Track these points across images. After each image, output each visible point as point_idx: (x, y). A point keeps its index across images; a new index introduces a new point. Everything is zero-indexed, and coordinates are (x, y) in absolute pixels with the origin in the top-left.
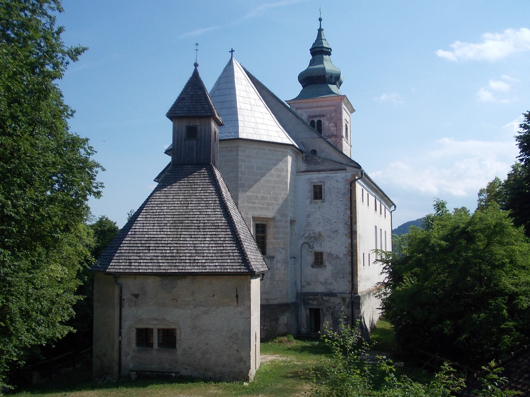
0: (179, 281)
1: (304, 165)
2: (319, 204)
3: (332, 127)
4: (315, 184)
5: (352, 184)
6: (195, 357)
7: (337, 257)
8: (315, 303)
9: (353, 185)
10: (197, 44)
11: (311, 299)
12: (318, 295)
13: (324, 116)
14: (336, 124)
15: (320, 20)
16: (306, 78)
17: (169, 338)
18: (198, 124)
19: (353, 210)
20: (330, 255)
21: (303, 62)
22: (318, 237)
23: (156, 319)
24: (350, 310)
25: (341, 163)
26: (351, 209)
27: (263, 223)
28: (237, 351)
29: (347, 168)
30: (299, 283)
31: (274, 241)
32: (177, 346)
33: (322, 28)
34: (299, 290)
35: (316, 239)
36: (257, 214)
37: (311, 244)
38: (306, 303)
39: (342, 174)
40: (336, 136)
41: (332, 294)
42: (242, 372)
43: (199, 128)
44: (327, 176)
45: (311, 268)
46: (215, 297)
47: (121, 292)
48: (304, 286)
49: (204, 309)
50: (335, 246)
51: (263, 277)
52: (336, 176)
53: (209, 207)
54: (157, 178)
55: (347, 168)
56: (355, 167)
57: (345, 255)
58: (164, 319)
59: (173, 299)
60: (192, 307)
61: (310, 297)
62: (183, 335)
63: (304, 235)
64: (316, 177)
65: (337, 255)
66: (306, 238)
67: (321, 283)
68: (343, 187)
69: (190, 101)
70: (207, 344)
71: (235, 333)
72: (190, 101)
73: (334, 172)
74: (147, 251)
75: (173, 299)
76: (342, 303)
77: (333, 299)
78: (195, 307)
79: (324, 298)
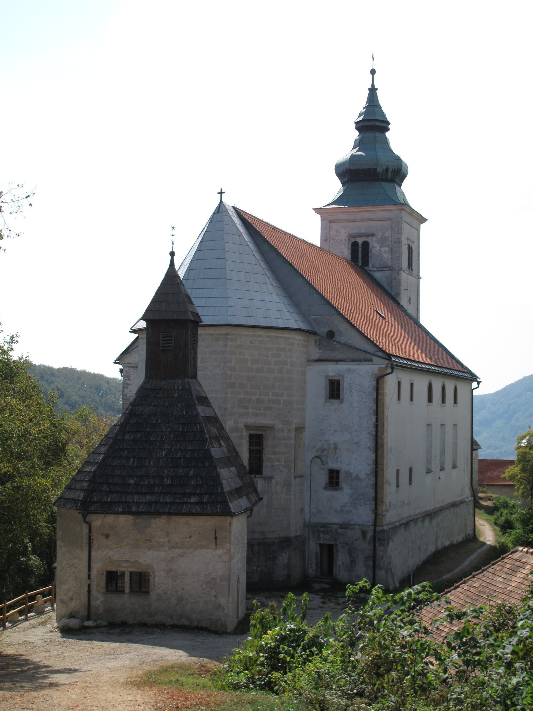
0: (153, 521)
1: (317, 350)
6: (170, 603)
7: (357, 478)
8: (328, 537)
9: (380, 381)
10: (173, 228)
13: (373, 235)
15: (373, 72)
16: (346, 170)
17: (141, 581)
19: (379, 416)
20: (348, 474)
21: (344, 144)
23: (127, 561)
27: (258, 432)
28: (215, 597)
31: (273, 456)
33: (376, 87)
34: (307, 519)
36: (251, 421)
40: (391, 269)
42: (220, 619)
46: (192, 538)
49: (179, 551)
50: (356, 462)
51: (251, 513)
54: (118, 359)
55: (374, 358)
57: (367, 475)
58: (137, 561)
60: (167, 548)
62: (156, 579)
64: (332, 370)
65: (357, 475)
68: (369, 384)
70: (183, 589)
71: (213, 578)
73: (356, 363)
78: (170, 549)
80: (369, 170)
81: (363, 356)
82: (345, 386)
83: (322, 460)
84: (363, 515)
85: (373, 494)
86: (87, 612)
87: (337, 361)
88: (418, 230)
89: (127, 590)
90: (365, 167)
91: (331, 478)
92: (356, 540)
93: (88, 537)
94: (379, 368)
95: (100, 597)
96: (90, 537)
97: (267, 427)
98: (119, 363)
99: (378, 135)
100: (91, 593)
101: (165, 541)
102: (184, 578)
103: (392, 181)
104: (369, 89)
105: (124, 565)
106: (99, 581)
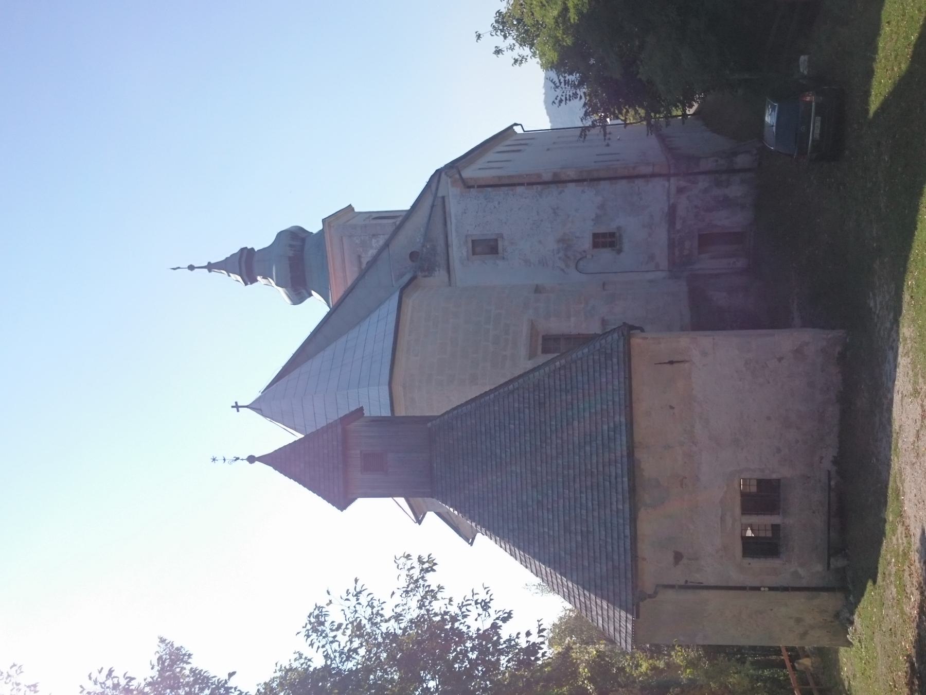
1: (437, 273)
3: (378, 242)
5: (468, 185)
6: (797, 442)
7: (602, 207)
10: (214, 460)
14: (374, 235)
15: (191, 268)
17: (763, 497)
18: (358, 452)
19: (516, 181)
20: (597, 219)
22: (566, 243)
23: (723, 519)
25: (433, 206)
27: (540, 341)
28: (780, 359)
29: (440, 194)
32: (774, 476)
33: (206, 264)
41: (672, 214)
47: (672, 587)
50: (581, 209)
53: (545, 486)
54: (467, 540)
55: (440, 194)
56: (439, 181)
61: (677, 253)
63: (563, 270)
64: (458, 251)
73: (448, 219)
74: (591, 537)
79: (678, 226)
81: (438, 211)
83: (580, 259)
85: (624, 182)
86: (822, 593)
87: (447, 245)
88: (360, 213)
89: (776, 519)
91: (604, 245)
95: (793, 570)
96: (682, 587)
98: (473, 539)
100: (786, 585)
103: (303, 240)
104: (210, 271)
106: (760, 569)
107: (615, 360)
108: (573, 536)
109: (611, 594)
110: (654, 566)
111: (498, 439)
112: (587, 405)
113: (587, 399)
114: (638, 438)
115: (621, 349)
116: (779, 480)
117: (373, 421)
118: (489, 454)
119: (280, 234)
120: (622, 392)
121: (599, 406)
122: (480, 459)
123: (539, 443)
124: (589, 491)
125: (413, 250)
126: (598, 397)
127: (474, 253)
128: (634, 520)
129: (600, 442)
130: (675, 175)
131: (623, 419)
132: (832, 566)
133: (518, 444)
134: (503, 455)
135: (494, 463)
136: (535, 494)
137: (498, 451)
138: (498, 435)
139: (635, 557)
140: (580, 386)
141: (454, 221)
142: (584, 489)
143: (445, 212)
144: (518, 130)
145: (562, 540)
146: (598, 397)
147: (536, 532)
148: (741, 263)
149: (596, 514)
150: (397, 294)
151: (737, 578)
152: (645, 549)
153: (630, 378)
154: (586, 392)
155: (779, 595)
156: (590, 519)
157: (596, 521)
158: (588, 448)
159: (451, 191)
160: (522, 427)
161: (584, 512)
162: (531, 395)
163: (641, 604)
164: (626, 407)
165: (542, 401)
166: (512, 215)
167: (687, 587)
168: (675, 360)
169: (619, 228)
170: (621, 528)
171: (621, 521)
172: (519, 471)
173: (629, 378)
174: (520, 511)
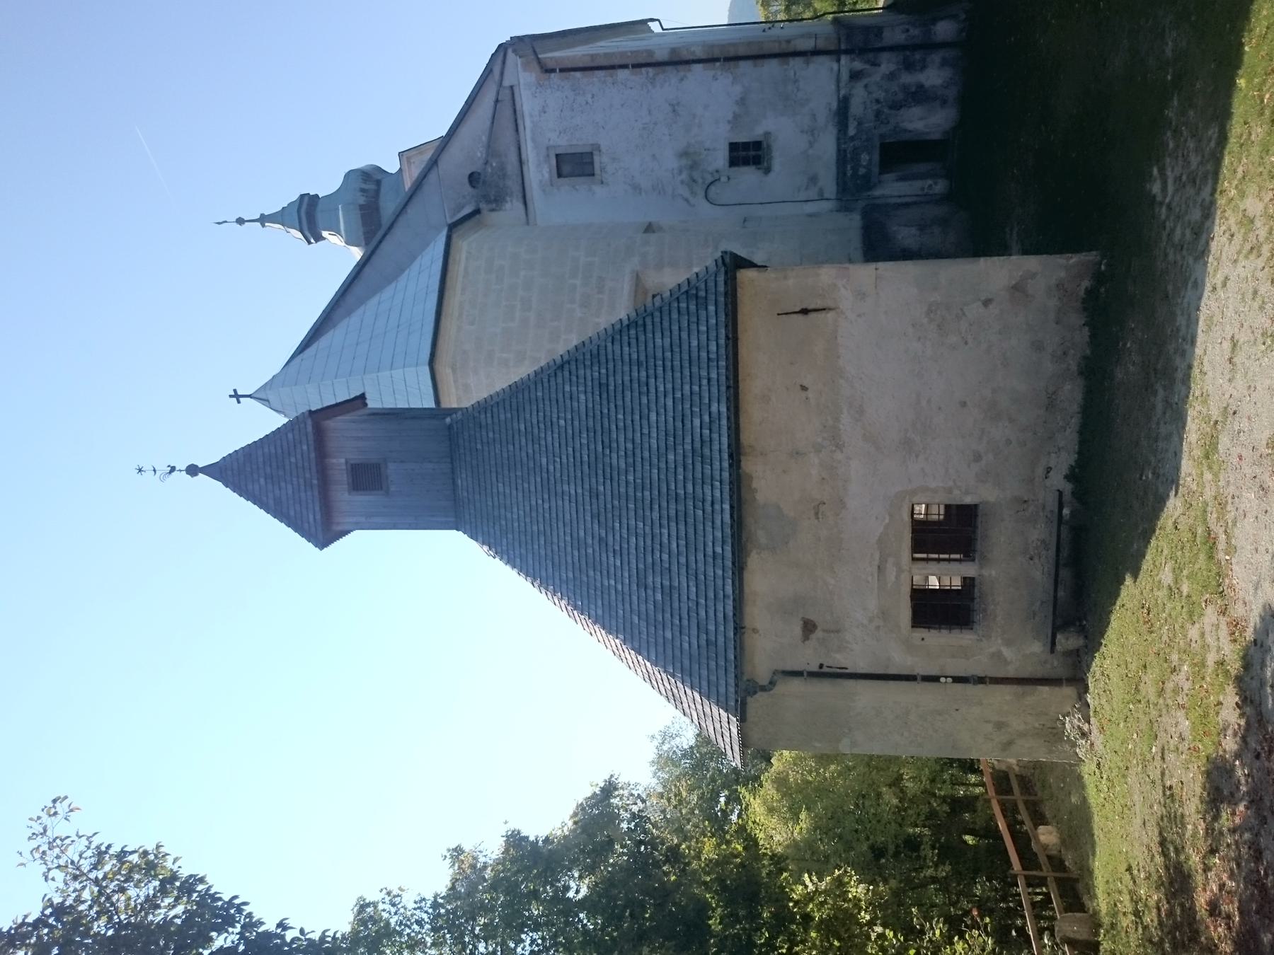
0: (760, 497)
1: (508, 206)
2: (605, 159)
4: (555, 175)
6: (1009, 442)
7: (742, 101)
8: (865, 158)
10: (140, 470)
11: (855, 170)
12: (845, 151)
15: (240, 221)
17: (949, 532)
18: (343, 461)
19: (616, 62)
20: (735, 121)
22: (691, 159)
24: (885, 56)
25: (497, 101)
26: (613, 67)
28: (987, 303)
30: (810, 208)
32: (968, 500)
35: (693, 166)
37: (710, 179)
38: (867, 183)
39: (524, 99)
41: (842, 112)
42: (1060, 286)
43: (356, 457)
44: (533, 140)
45: (772, 175)
47: (798, 674)
48: (821, 192)
49: (846, 419)
52: (531, 116)
55: (506, 83)
56: (504, 62)
58: (880, 541)
59: (817, 514)
60: (839, 456)
61: (849, 173)
64: (538, 172)
66: (693, 193)
67: (811, 144)
68: (558, 92)
69: (283, 484)
71: (929, 311)
72: (283, 484)
73: (520, 122)
75: (817, 514)
76: (865, 81)
77: (856, 108)
78: (839, 447)
80: (363, 216)
81: (506, 111)
82: (563, 143)
84: (820, 82)
86: (1040, 688)
89: (970, 570)
90: (360, 222)
91: (746, 162)
92: (870, 93)
93: (815, 680)
94: (525, 70)
95: (993, 650)
97: (637, 285)
99: (320, 207)
101: (817, 461)
102: (929, 401)
103: (378, 183)
105: (893, 578)
107: (712, 308)
108: (650, 592)
109: (704, 684)
110: (771, 642)
111: (543, 442)
112: (669, 386)
113: (669, 373)
114: (747, 437)
115: (721, 288)
116: (976, 506)
117: (374, 414)
118: (531, 465)
119: (349, 175)
120: (722, 363)
121: (687, 387)
122: (519, 473)
123: (600, 448)
124: (673, 524)
125: (474, 169)
126: (687, 372)
127: (560, 175)
128: (739, 567)
129: (688, 447)
130: (846, 52)
131: (724, 409)
132: (1058, 647)
133: (570, 449)
134: (551, 468)
135: (539, 480)
136: (596, 527)
137: (544, 461)
138: (543, 435)
139: (739, 629)
140: (659, 354)
141: (528, 124)
142: (665, 522)
143: (515, 111)
144: (655, 27)
145: (635, 598)
146: (687, 372)
147: (599, 585)
148: (940, 187)
149: (683, 560)
150: (445, 232)
151: (901, 661)
152: (756, 615)
153: (736, 340)
154: (668, 364)
155: (970, 689)
156: (674, 568)
157: (683, 571)
158: (671, 457)
159: (522, 76)
160: (576, 423)
161: (665, 557)
162: (588, 372)
163: (749, 699)
164: (728, 387)
165: (604, 381)
166: (611, 117)
167: (821, 674)
168: (810, 307)
169: (767, 134)
170: (720, 582)
171: (720, 572)
172: (573, 492)
173: (733, 340)
174: (576, 553)
